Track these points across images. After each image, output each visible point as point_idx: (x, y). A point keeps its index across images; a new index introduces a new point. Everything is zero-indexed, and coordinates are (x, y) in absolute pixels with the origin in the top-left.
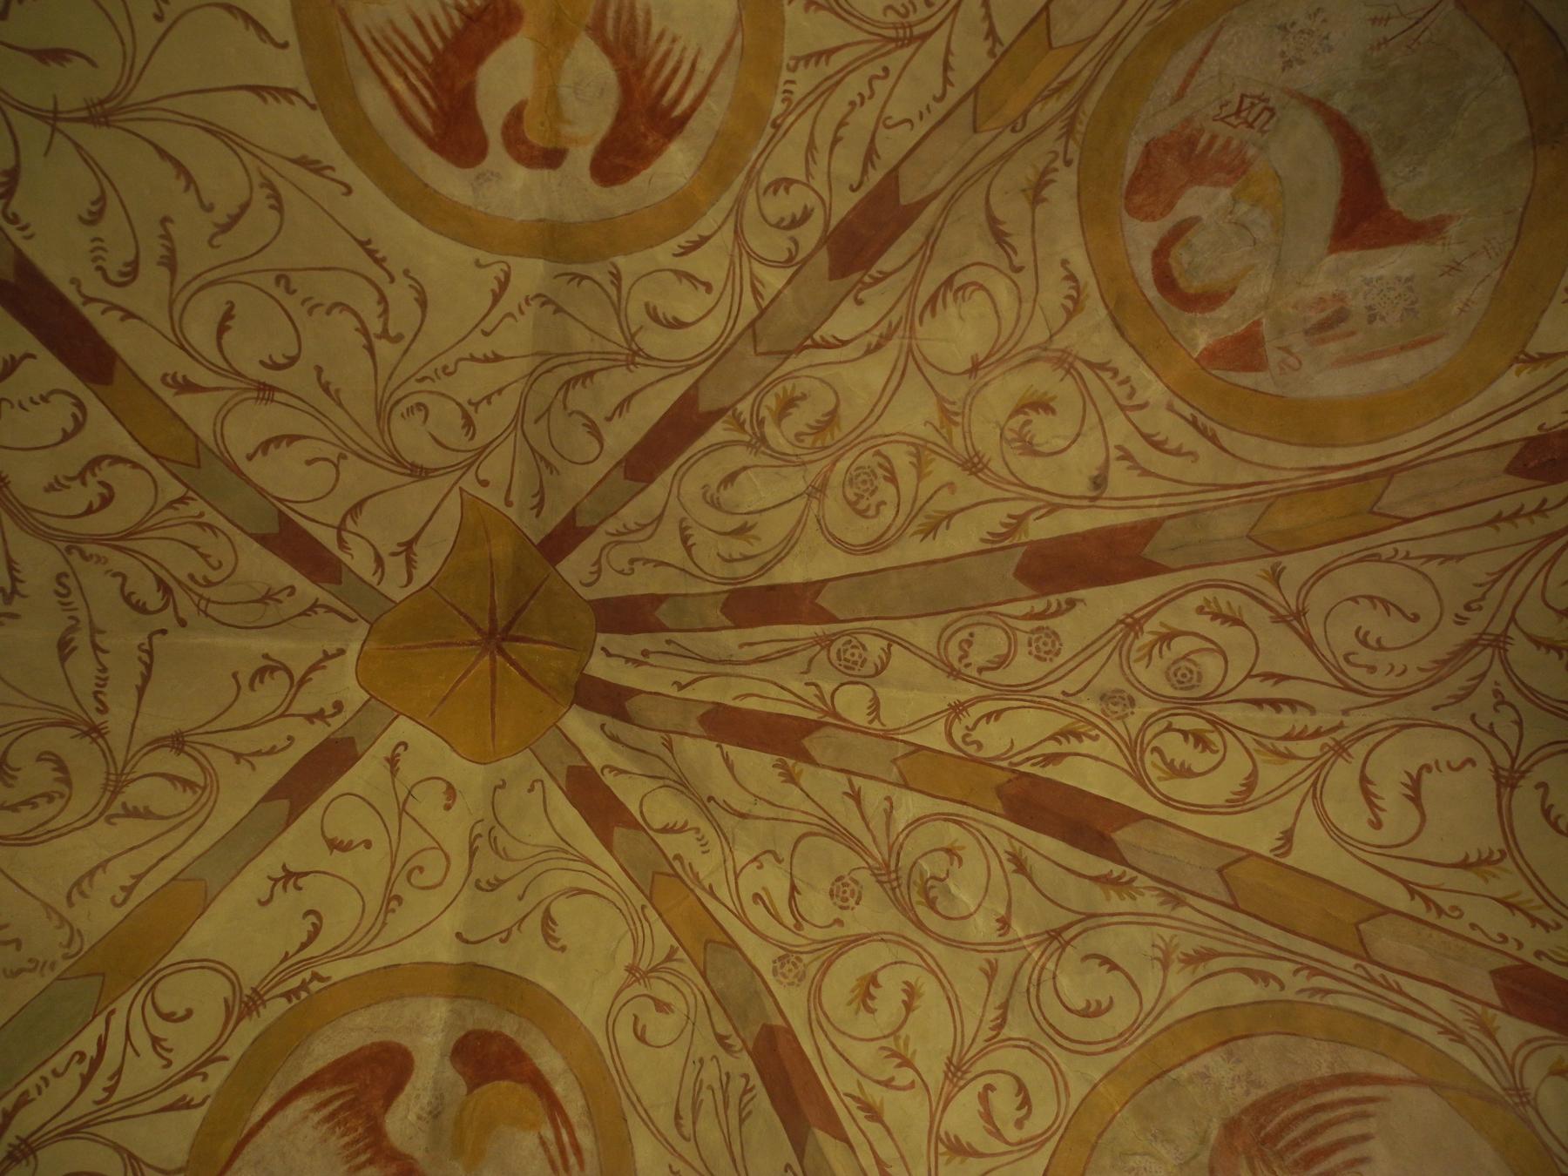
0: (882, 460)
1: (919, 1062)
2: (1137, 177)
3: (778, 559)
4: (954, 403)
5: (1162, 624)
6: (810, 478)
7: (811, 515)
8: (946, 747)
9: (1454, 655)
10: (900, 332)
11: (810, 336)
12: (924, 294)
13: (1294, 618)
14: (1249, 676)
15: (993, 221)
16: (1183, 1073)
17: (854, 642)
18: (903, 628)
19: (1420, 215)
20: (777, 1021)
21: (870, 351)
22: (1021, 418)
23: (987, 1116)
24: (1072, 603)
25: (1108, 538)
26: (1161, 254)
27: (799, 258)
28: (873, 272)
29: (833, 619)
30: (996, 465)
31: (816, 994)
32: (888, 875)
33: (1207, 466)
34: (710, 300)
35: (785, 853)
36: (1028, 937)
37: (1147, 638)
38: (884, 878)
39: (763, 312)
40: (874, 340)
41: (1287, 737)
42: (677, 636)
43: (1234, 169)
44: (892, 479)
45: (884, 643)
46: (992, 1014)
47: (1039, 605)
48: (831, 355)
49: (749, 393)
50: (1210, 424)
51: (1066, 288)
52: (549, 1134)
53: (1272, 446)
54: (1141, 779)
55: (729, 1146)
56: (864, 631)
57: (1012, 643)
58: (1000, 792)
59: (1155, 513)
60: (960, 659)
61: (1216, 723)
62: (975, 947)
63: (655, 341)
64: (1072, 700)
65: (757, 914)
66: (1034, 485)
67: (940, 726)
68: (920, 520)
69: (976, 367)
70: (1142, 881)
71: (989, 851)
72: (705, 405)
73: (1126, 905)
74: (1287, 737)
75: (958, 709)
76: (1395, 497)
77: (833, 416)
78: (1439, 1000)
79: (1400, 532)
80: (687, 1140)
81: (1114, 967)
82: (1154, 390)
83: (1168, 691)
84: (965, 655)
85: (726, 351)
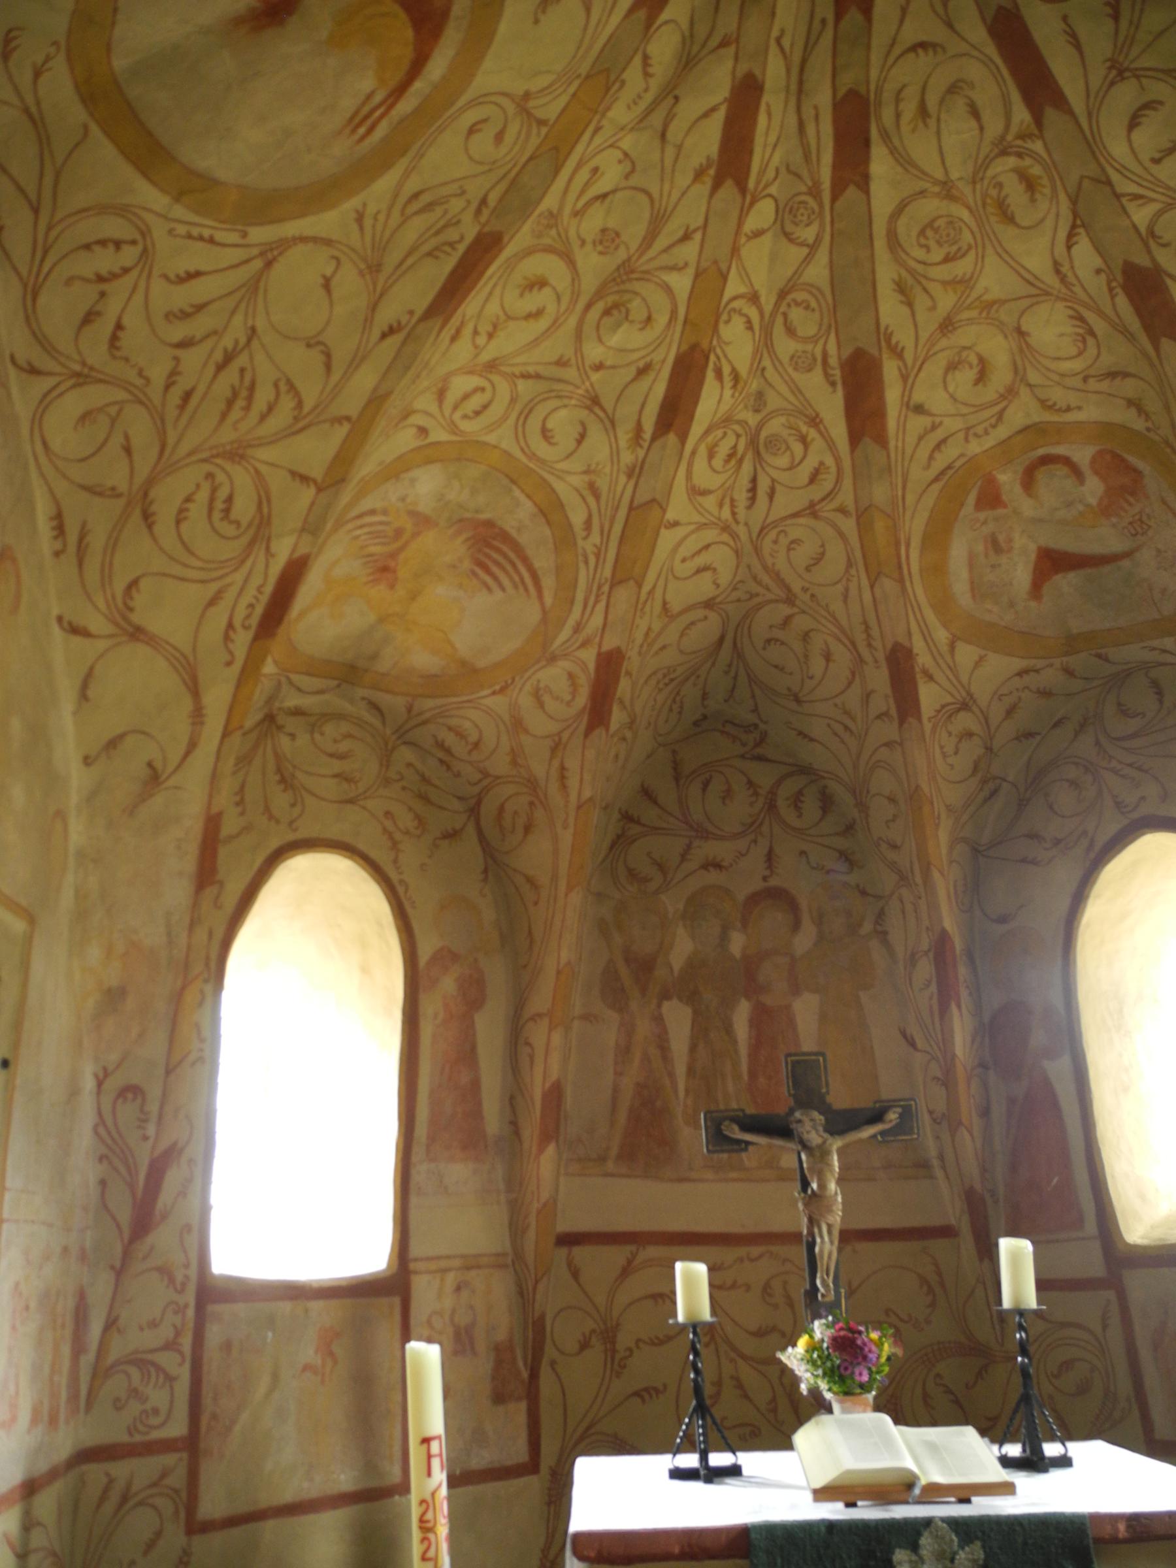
0: (963, 251)
1: (494, 343)
2: (1123, 460)
3: (893, 151)
4: (997, 311)
5: (813, 440)
6: (960, 184)
7: (928, 185)
8: (728, 294)
9: (782, 581)
10: (1064, 290)
11: (1083, 226)
12: (1087, 314)
13: (812, 510)
14: (773, 481)
15: (1126, 375)
16: (517, 493)
17: (813, 217)
18: (822, 257)
19: (1046, 588)
20: (506, 239)
21: (1057, 266)
22: (975, 361)
23: (466, 397)
24: (833, 384)
25: (880, 413)
26: (1067, 461)
27: (1151, 242)
28: (1119, 290)
29: (834, 199)
30: (944, 343)
31: (529, 252)
32: (625, 273)
33: (919, 475)
34: (1145, 157)
35: (634, 181)
36: (592, 385)
37: (804, 429)
38: (622, 271)
39: (1118, 196)
40: (1064, 270)
41: (732, 500)
42: (829, 34)
43: (1106, 509)
44: (947, 259)
45: (811, 241)
46: (531, 369)
47: (833, 361)
48: (1062, 235)
49: (1050, 155)
50: (946, 477)
51: (1062, 404)
52: (378, 98)
53: (926, 514)
54: (707, 432)
55: (409, 254)
56: (822, 225)
57: (805, 340)
58: (694, 347)
59: (892, 444)
60: (794, 300)
61: (741, 461)
62: (578, 350)
63: (1126, 95)
64: (759, 373)
65: (584, 175)
66: (925, 366)
67: (742, 289)
68: (910, 281)
69: (1021, 333)
70: (641, 453)
71: (652, 348)
72: (1050, 114)
73: (623, 443)
74: (732, 500)
75: (754, 298)
76: (888, 585)
77: (1009, 218)
78: (597, 620)
79: (865, 582)
80: (402, 214)
81: (579, 442)
82: (975, 447)
83: (764, 434)
84: (797, 304)
85: (1093, 153)
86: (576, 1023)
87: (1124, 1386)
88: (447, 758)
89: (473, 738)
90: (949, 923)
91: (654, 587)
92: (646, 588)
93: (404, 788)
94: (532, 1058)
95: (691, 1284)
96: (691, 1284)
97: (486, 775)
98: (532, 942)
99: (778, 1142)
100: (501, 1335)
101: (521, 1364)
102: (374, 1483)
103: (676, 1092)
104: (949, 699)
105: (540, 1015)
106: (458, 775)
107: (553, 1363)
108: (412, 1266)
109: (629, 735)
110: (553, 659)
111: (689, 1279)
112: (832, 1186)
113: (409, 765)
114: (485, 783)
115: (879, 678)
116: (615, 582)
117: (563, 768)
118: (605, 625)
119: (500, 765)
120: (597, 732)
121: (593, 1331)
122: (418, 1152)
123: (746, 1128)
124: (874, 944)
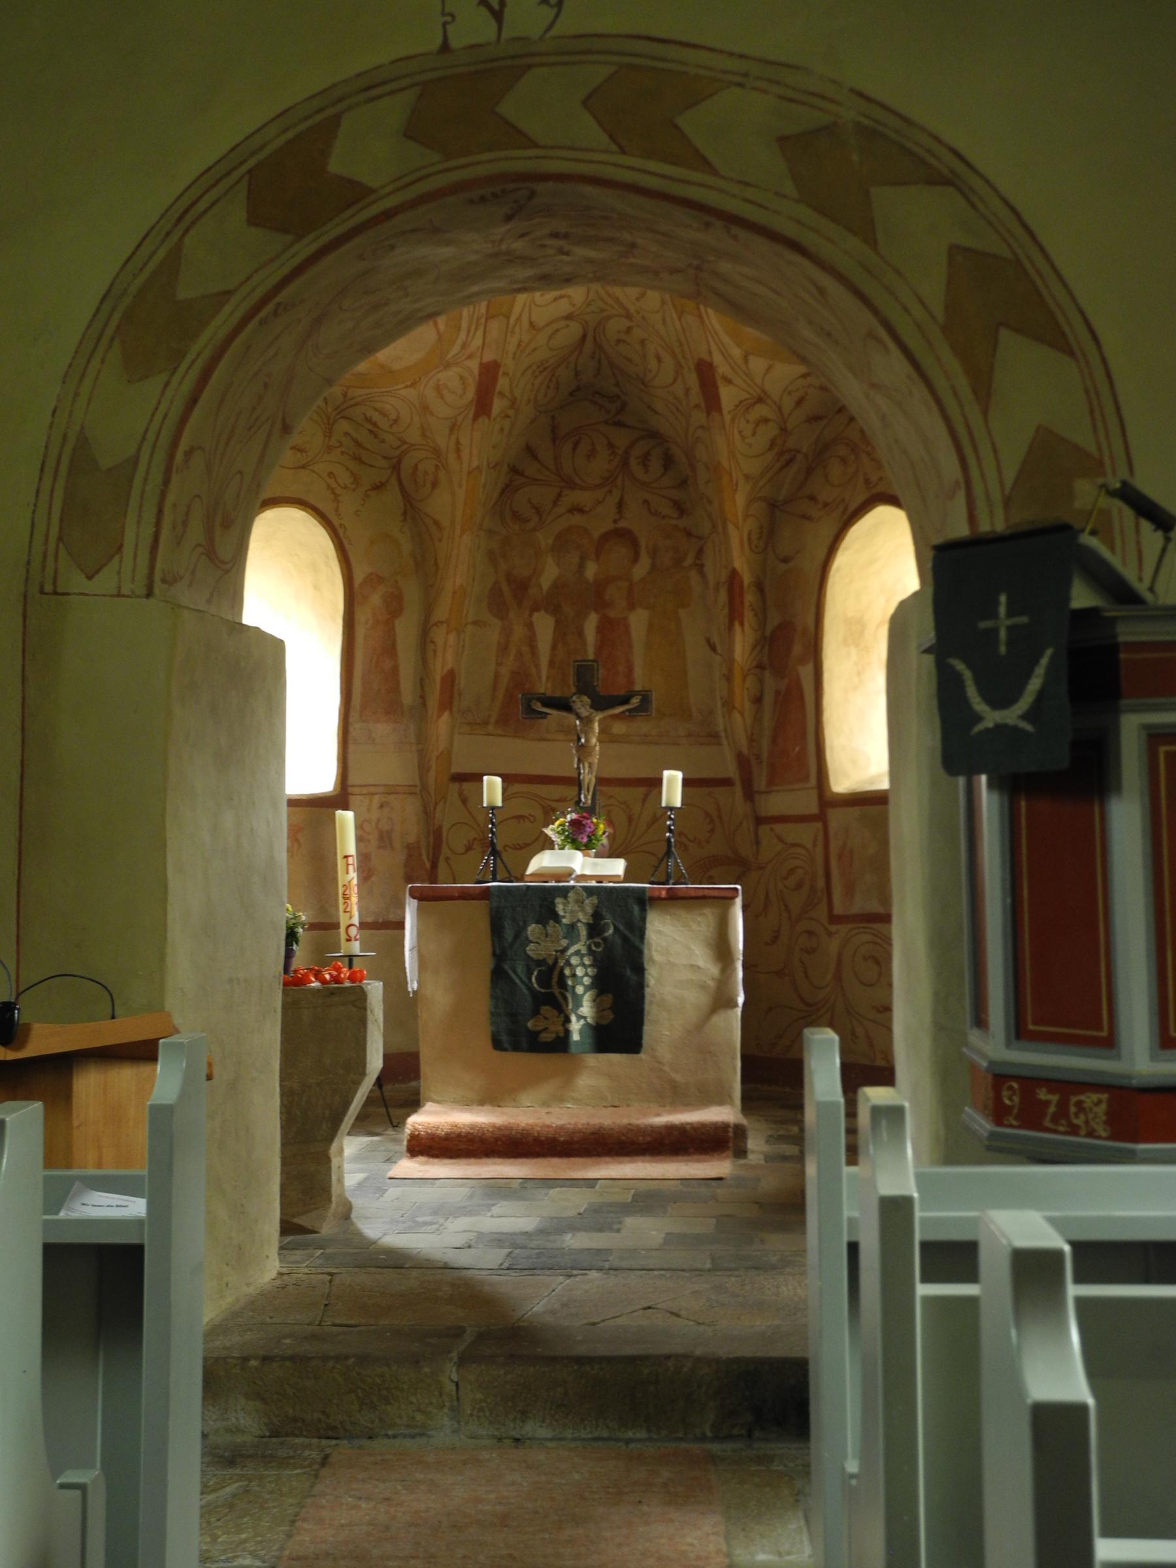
78: (477, 342)
79: (675, 316)
86: (469, 627)
87: (821, 883)
88: (375, 429)
89: (393, 416)
90: (739, 563)
91: (521, 315)
92: (513, 318)
93: (342, 453)
94: (435, 652)
95: (493, 789)
96: (493, 789)
97: (405, 442)
98: (437, 569)
99: (564, 714)
100: (412, 839)
101: (425, 857)
102: (327, 920)
103: (540, 677)
104: (748, 396)
105: (441, 622)
106: (383, 441)
107: (447, 859)
108: (350, 790)
109: (511, 412)
110: (448, 366)
111: (490, 784)
112: (594, 741)
113: (347, 434)
114: (405, 447)
115: (693, 380)
116: (489, 317)
117: (458, 443)
118: (484, 344)
119: (413, 436)
120: (481, 420)
121: (475, 839)
122: (354, 716)
123: (545, 705)
124: (693, 574)
